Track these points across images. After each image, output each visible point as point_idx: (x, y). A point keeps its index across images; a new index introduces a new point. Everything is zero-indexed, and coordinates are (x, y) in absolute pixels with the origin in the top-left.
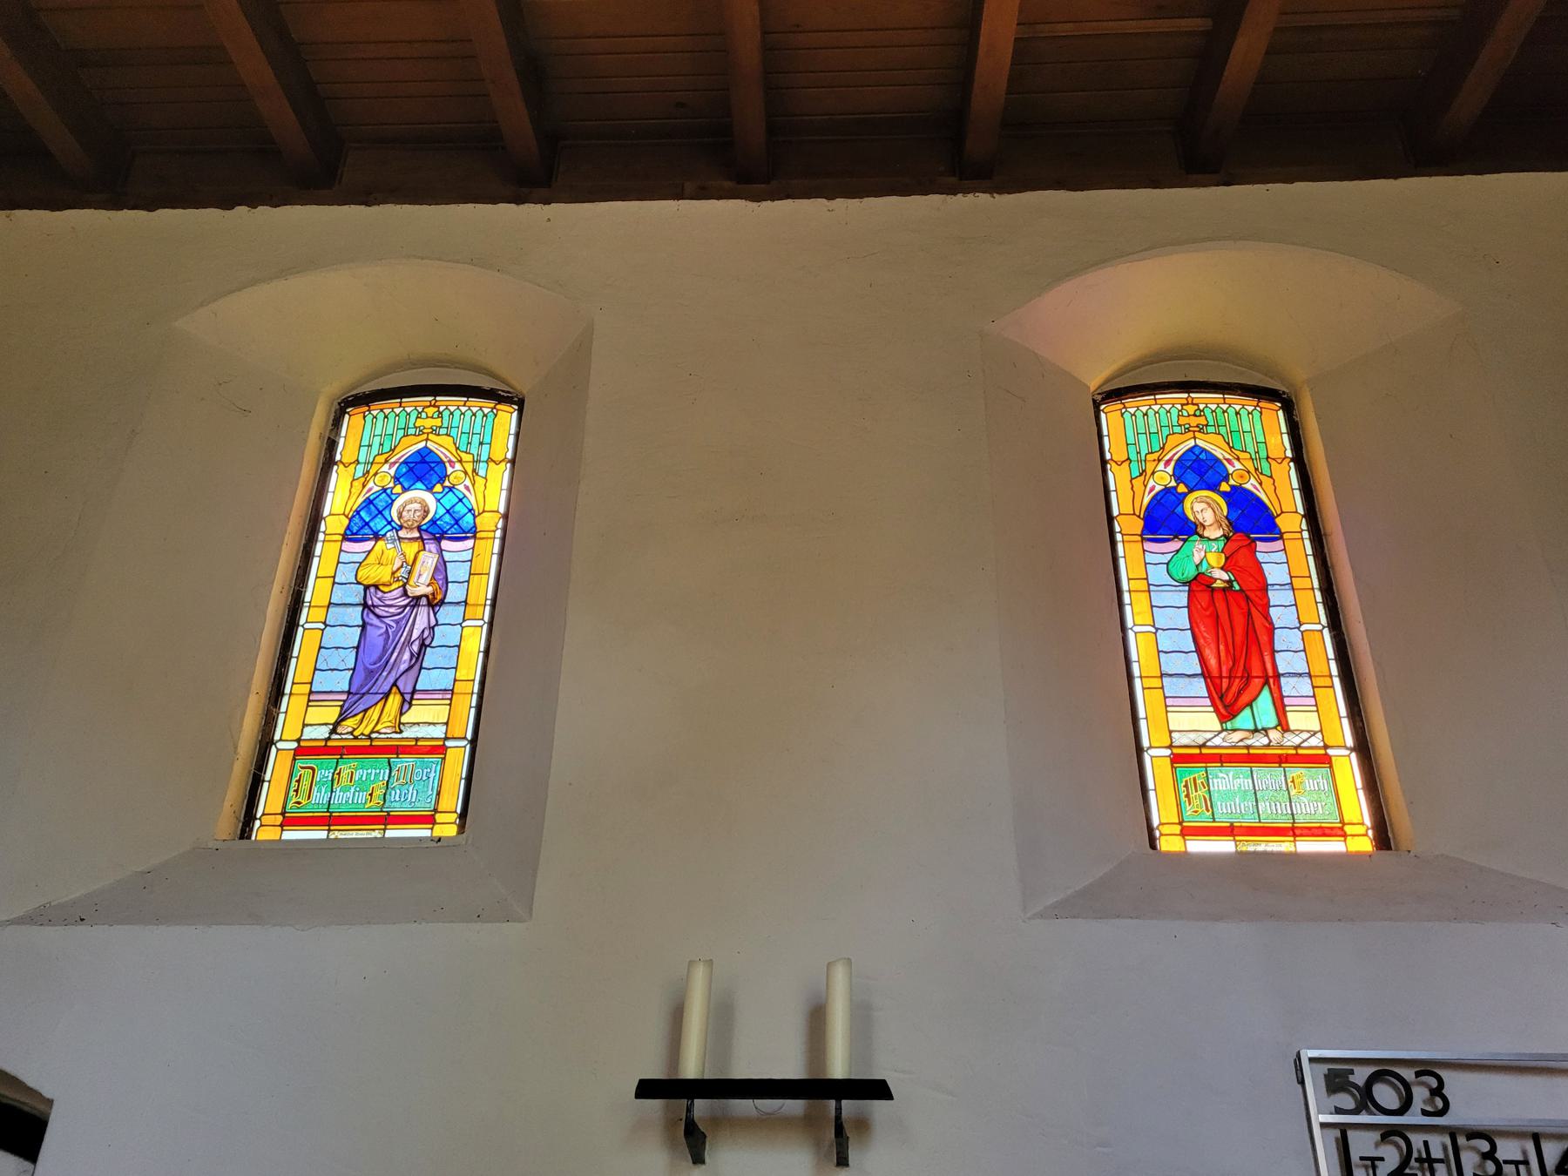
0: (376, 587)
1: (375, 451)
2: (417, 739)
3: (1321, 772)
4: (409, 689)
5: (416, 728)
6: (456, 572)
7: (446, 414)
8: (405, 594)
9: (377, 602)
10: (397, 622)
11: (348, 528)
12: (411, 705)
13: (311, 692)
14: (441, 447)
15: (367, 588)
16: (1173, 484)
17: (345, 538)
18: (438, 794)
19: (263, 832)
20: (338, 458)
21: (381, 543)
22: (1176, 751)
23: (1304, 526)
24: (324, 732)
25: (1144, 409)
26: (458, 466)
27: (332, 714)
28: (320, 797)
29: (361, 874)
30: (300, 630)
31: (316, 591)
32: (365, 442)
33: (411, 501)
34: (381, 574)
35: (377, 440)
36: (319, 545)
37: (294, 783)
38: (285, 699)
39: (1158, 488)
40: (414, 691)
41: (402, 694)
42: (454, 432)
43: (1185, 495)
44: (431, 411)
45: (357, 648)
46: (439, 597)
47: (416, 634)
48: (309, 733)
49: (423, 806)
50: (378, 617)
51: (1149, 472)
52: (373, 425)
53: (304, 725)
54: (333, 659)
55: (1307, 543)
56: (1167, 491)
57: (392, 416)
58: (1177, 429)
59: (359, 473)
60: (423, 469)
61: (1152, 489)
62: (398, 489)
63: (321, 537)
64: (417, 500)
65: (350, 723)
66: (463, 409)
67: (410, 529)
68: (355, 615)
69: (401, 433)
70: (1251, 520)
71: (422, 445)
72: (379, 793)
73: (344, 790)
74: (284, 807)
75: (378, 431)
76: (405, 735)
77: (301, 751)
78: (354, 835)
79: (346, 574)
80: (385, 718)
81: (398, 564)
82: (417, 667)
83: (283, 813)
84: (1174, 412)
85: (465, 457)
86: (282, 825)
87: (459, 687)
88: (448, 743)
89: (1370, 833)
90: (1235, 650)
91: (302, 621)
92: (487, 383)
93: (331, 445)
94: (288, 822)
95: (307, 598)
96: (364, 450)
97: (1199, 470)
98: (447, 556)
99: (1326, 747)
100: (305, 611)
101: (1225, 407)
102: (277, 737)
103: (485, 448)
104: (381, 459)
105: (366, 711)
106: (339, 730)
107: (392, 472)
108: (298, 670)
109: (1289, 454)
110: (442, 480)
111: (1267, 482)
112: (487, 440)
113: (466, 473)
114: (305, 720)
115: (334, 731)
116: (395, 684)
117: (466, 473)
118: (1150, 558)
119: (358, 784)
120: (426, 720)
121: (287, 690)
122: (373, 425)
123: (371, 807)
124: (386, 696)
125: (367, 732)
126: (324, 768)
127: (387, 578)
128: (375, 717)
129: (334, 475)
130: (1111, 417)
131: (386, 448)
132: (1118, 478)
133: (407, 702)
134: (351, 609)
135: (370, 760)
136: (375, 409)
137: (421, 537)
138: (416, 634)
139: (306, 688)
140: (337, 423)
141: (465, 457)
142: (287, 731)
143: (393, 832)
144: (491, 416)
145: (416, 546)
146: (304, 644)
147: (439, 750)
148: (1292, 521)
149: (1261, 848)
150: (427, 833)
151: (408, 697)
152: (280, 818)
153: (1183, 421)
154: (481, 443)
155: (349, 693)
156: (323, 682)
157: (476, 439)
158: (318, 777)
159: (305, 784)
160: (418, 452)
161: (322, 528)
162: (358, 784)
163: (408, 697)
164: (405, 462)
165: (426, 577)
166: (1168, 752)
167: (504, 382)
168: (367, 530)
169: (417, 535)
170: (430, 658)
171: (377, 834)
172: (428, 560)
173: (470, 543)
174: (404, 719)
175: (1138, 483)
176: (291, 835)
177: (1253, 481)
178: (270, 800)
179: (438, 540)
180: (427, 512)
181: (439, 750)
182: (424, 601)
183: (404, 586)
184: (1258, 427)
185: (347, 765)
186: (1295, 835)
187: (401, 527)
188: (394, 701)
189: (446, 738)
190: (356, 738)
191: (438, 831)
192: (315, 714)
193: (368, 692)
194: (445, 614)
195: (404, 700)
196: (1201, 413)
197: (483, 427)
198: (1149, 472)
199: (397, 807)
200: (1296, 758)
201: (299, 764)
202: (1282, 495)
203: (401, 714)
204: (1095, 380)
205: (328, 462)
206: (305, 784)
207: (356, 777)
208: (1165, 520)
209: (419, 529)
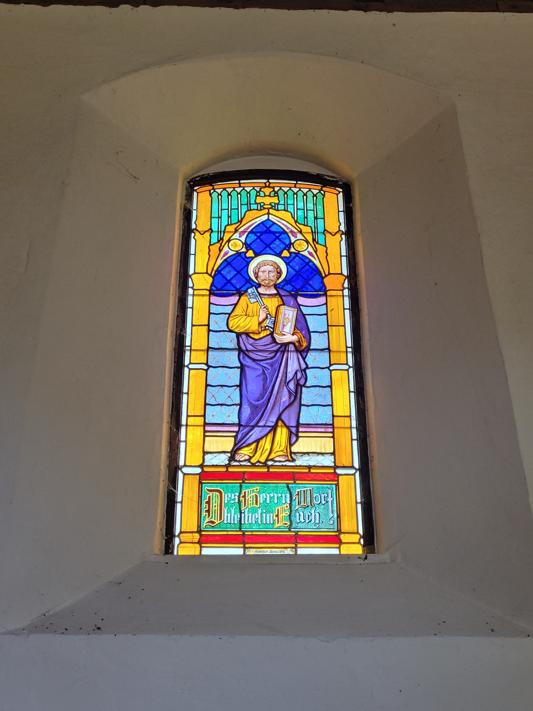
0: (247, 334)
1: (225, 222)
2: (309, 467)
3: (329, 488)
4: (294, 424)
5: (306, 457)
6: (313, 323)
7: (281, 193)
8: (274, 340)
9: (250, 347)
10: (272, 365)
11: (212, 285)
12: (298, 437)
13: (205, 424)
14: (282, 219)
15: (238, 335)
16: (244, 250)
17: (211, 293)
18: (339, 517)
19: (183, 549)
20: (194, 226)
21: (243, 298)
22: (206, 469)
23: (346, 285)
24: (223, 459)
25: (305, 191)
26: (299, 236)
27: (228, 444)
28: (230, 516)
29: (265, 590)
30: (186, 370)
31: (195, 338)
32: (215, 214)
33: (264, 263)
34: (252, 324)
35: (225, 214)
36: (190, 299)
37: (204, 505)
38: (183, 429)
39: (231, 253)
40: (298, 425)
41: (288, 427)
42: (290, 208)
43: (252, 258)
44: (267, 191)
45: (240, 386)
46: (305, 344)
47: (290, 376)
48: (210, 460)
49: (327, 528)
50: (254, 360)
51: (225, 239)
52: (220, 202)
53: (205, 453)
54: (221, 395)
55: (347, 300)
56: (238, 254)
57: (234, 194)
58: (254, 207)
59: (214, 239)
60: (267, 238)
61: (226, 253)
62: (250, 254)
63: (190, 291)
64: (266, 266)
65: (246, 452)
66: (295, 190)
67: (268, 286)
68: (233, 358)
69: (244, 208)
70: (303, 280)
71: (265, 217)
72: (284, 514)
73: (254, 511)
74: (199, 526)
75: (225, 206)
76: (298, 463)
77: (205, 476)
78: (277, 552)
79: (218, 323)
80: (276, 448)
81: (262, 316)
82: (296, 404)
83: (199, 531)
84: (253, 193)
85: (305, 229)
86: (200, 542)
87: (338, 422)
88: (339, 471)
89: (362, 541)
90: (270, 386)
91: (187, 362)
92: (313, 170)
93: (187, 215)
94: (204, 540)
95: (188, 343)
96: (215, 221)
97: (267, 238)
98: (305, 310)
99: (336, 467)
100: (187, 353)
101: (295, 190)
102: (181, 463)
103: (320, 222)
104: (231, 228)
105: (258, 441)
106: (237, 457)
107: (243, 239)
108: (191, 403)
109: (343, 228)
110: (288, 246)
111: (321, 249)
112: (320, 215)
113: (307, 242)
114: (202, 447)
115: (232, 459)
116: (279, 418)
117: (307, 242)
118: (214, 309)
119: (266, 508)
120: (313, 449)
121: (184, 422)
122: (220, 202)
123: (280, 526)
124: (274, 429)
125: (263, 460)
126: (230, 492)
127: (255, 327)
128: (268, 446)
129: (193, 241)
130: (202, 199)
131: (234, 220)
132: (199, 245)
133: (294, 435)
134: (228, 353)
135: (272, 484)
136: (219, 187)
137: (278, 294)
138: (290, 376)
139: (200, 421)
140: (189, 197)
141: (305, 229)
142: (189, 456)
143: (304, 550)
144: (320, 196)
145: (276, 301)
146: (192, 381)
147: (332, 476)
148: (337, 283)
149: (268, 552)
150: (335, 552)
151: (294, 430)
152: (197, 536)
153: (259, 200)
154: (316, 218)
155: (239, 425)
156: (215, 415)
157: (311, 215)
158: (225, 500)
159: (215, 502)
160: (262, 223)
161: (190, 284)
162: (266, 508)
163: (294, 430)
164: (251, 232)
165: (289, 328)
166: (199, 470)
167: (333, 171)
168: (229, 286)
169: (275, 292)
170: (307, 396)
171: (288, 552)
172: (289, 314)
173: (322, 300)
174: (294, 449)
175: (215, 249)
176: (208, 551)
177: (310, 249)
178: (185, 519)
179: (295, 297)
180: (280, 273)
181: (332, 476)
182: (291, 347)
183: (272, 334)
184: (320, 207)
185: (251, 490)
186: (244, 543)
187: (259, 285)
188: (282, 434)
189: (336, 467)
190: (253, 465)
191: (345, 550)
192: (212, 444)
193: (256, 425)
194: (312, 359)
195: (290, 433)
196: (276, 194)
197: (315, 204)
198: (225, 239)
199: (306, 528)
200: (309, 474)
201: (205, 487)
202: (332, 258)
203: (291, 445)
204: (187, 168)
205: (187, 232)
206: (215, 502)
207: (261, 500)
208: (231, 280)
209: (276, 286)
